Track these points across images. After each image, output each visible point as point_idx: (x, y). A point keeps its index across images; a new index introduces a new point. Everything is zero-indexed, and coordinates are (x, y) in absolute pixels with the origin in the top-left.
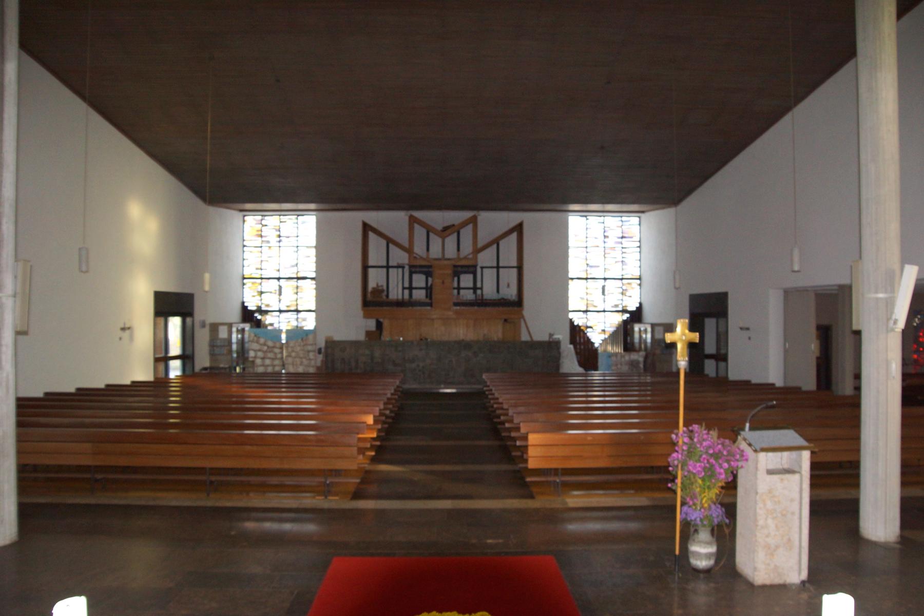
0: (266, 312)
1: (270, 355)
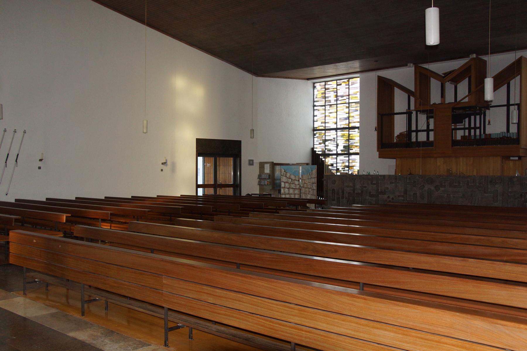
0: (329, 155)
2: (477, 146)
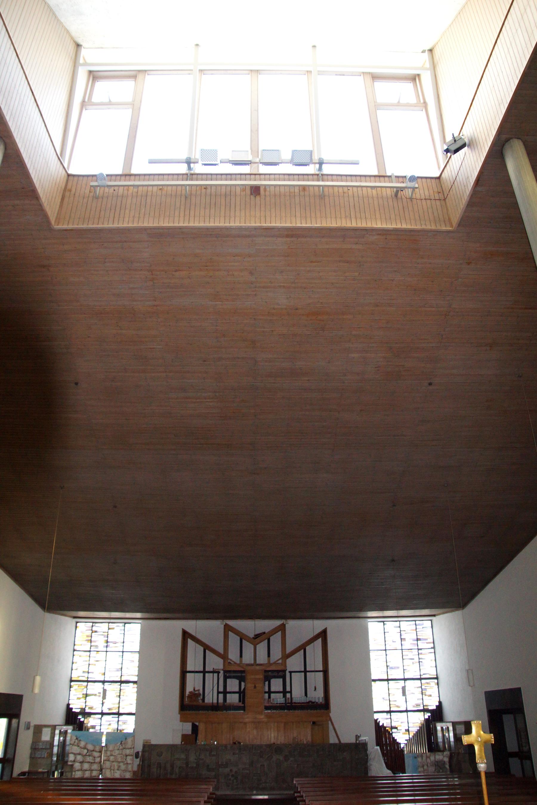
0: (90, 714)
1: (89, 759)
2: (288, 711)
